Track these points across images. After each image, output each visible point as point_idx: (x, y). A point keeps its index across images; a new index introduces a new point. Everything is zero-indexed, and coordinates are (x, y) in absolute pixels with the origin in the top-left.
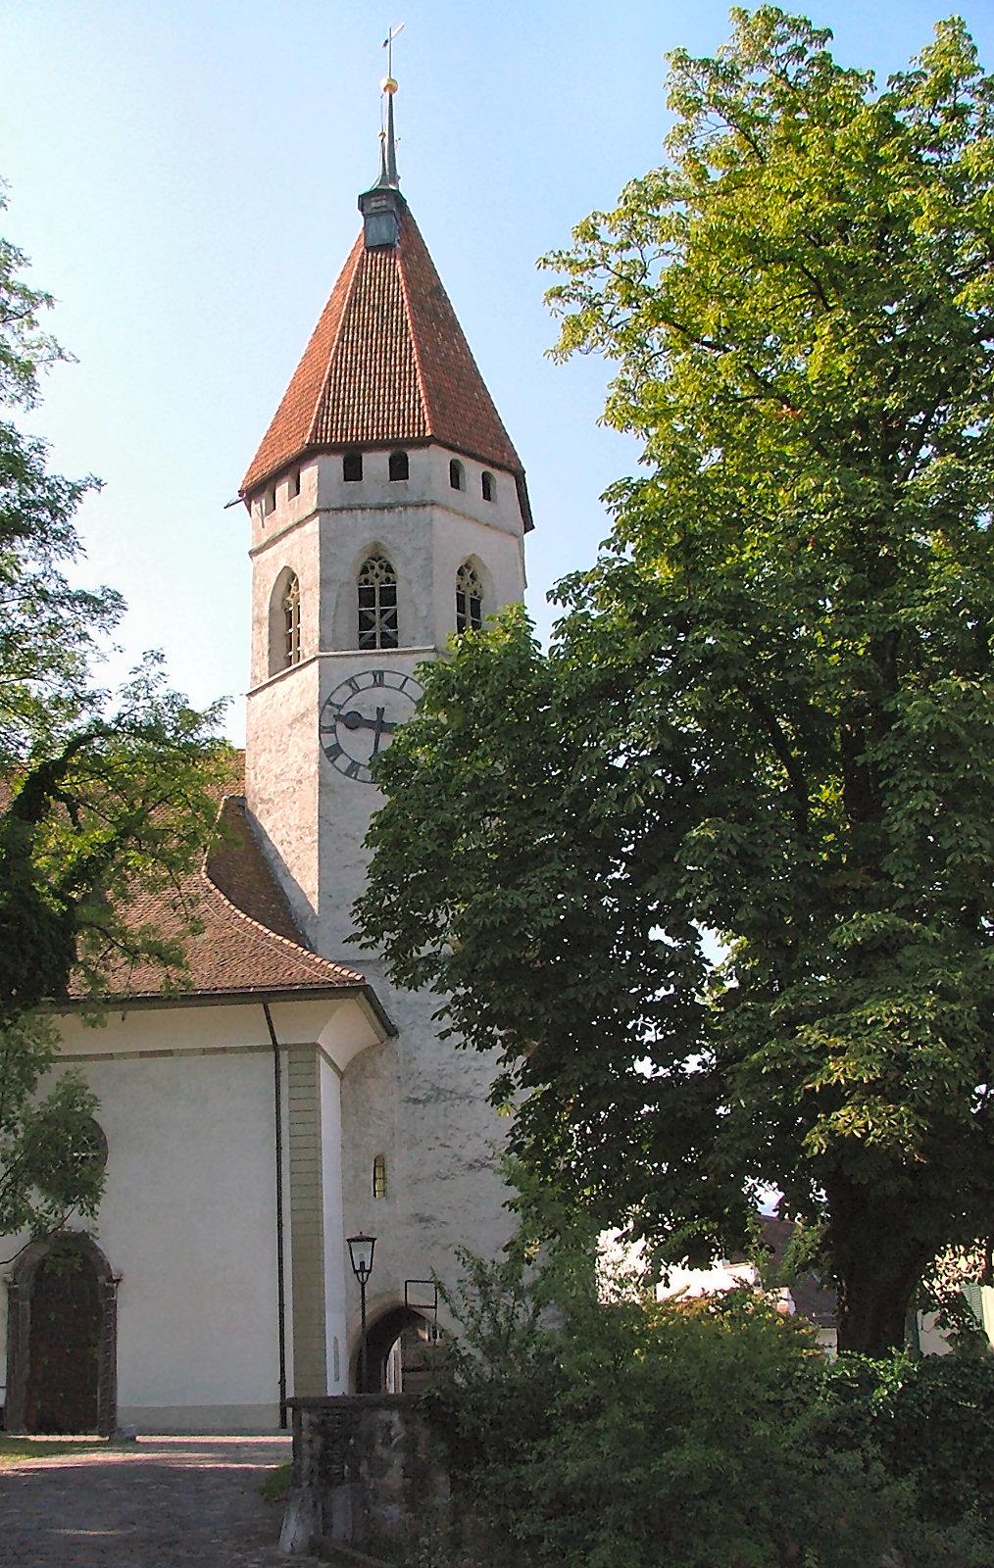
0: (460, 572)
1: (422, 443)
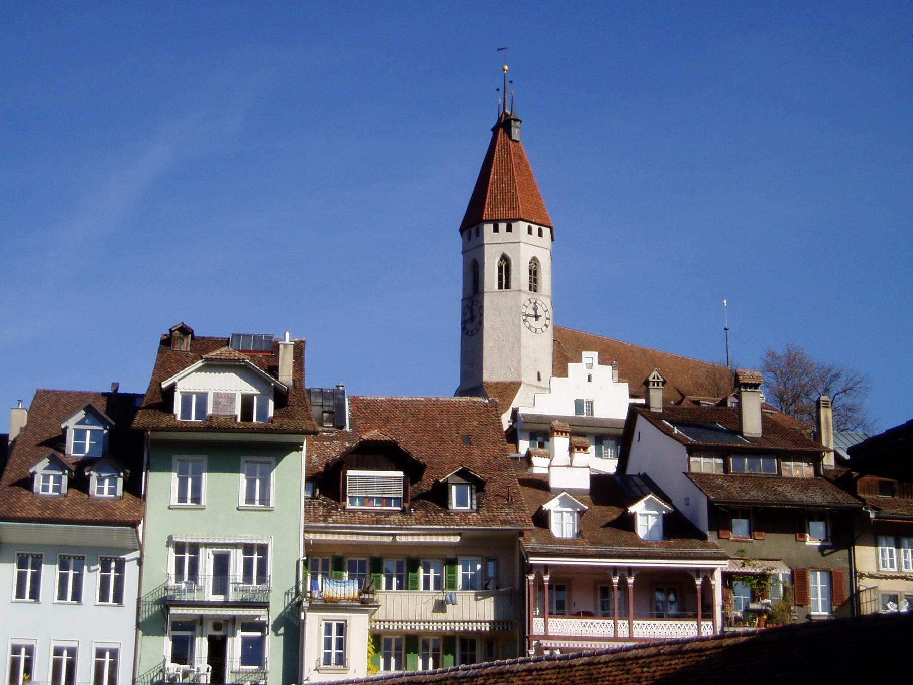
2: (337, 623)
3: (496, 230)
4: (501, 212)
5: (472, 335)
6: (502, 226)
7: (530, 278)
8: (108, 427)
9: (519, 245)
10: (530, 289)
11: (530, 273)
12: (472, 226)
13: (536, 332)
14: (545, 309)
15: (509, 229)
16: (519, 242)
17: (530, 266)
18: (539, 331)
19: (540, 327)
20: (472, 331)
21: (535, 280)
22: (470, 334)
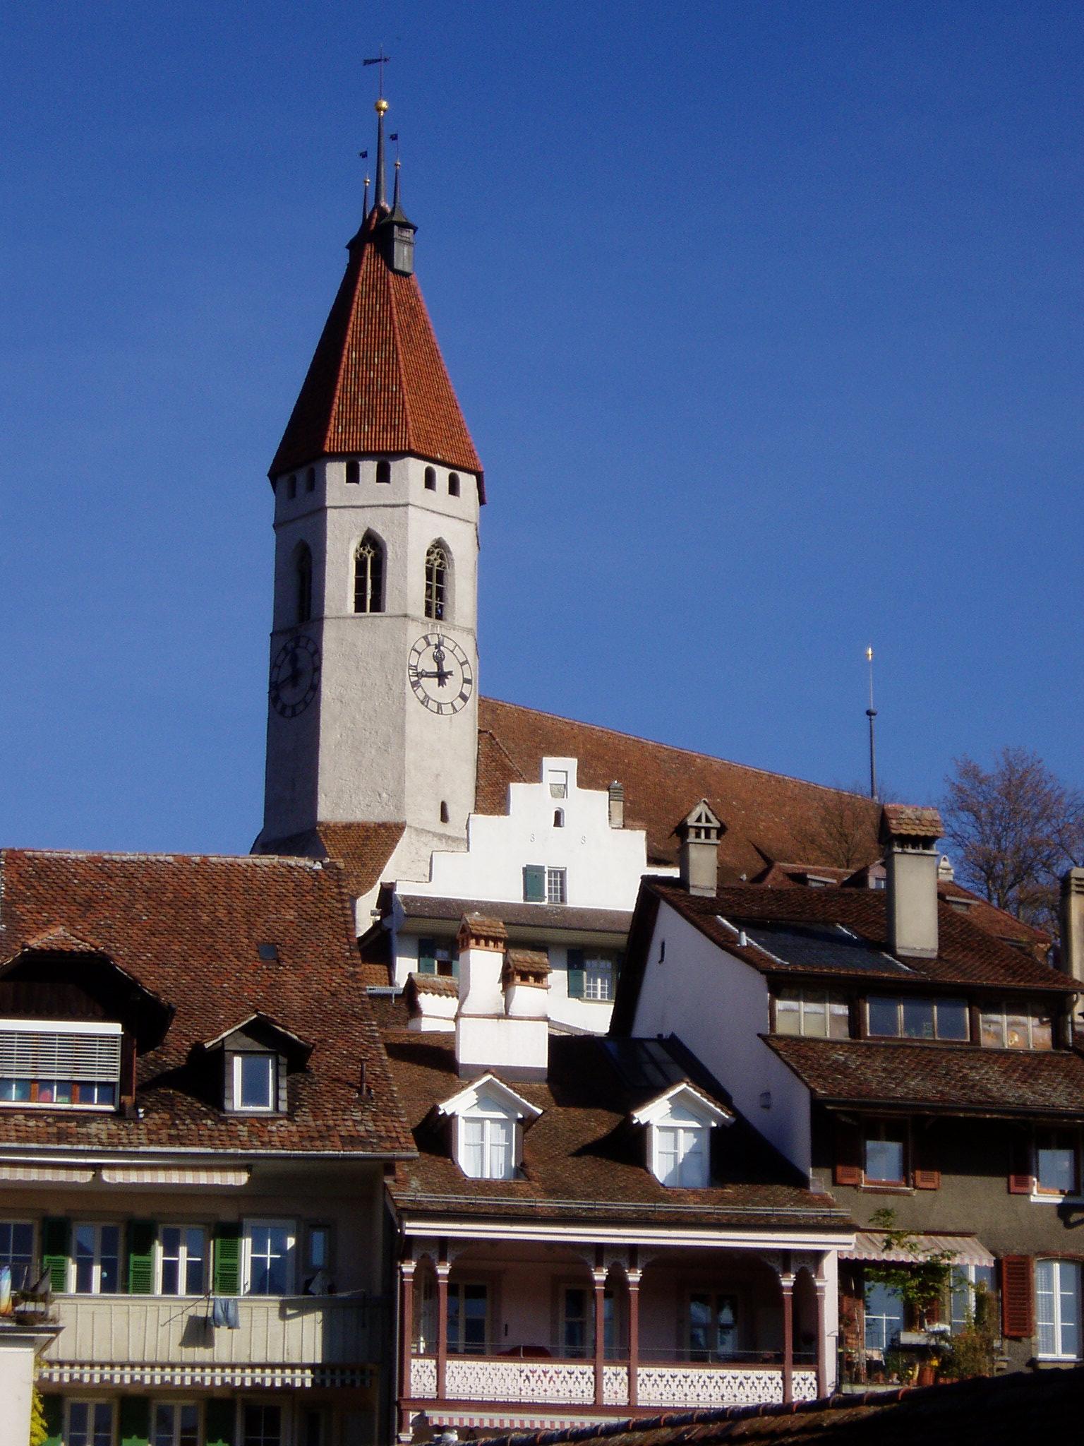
3: (353, 476)
4: (367, 437)
5: (294, 714)
6: (368, 468)
7: (429, 587)
10: (428, 614)
11: (429, 577)
13: (439, 710)
15: (383, 475)
16: (406, 505)
17: (428, 562)
18: (447, 709)
20: (294, 707)
21: (440, 594)
22: (288, 712)
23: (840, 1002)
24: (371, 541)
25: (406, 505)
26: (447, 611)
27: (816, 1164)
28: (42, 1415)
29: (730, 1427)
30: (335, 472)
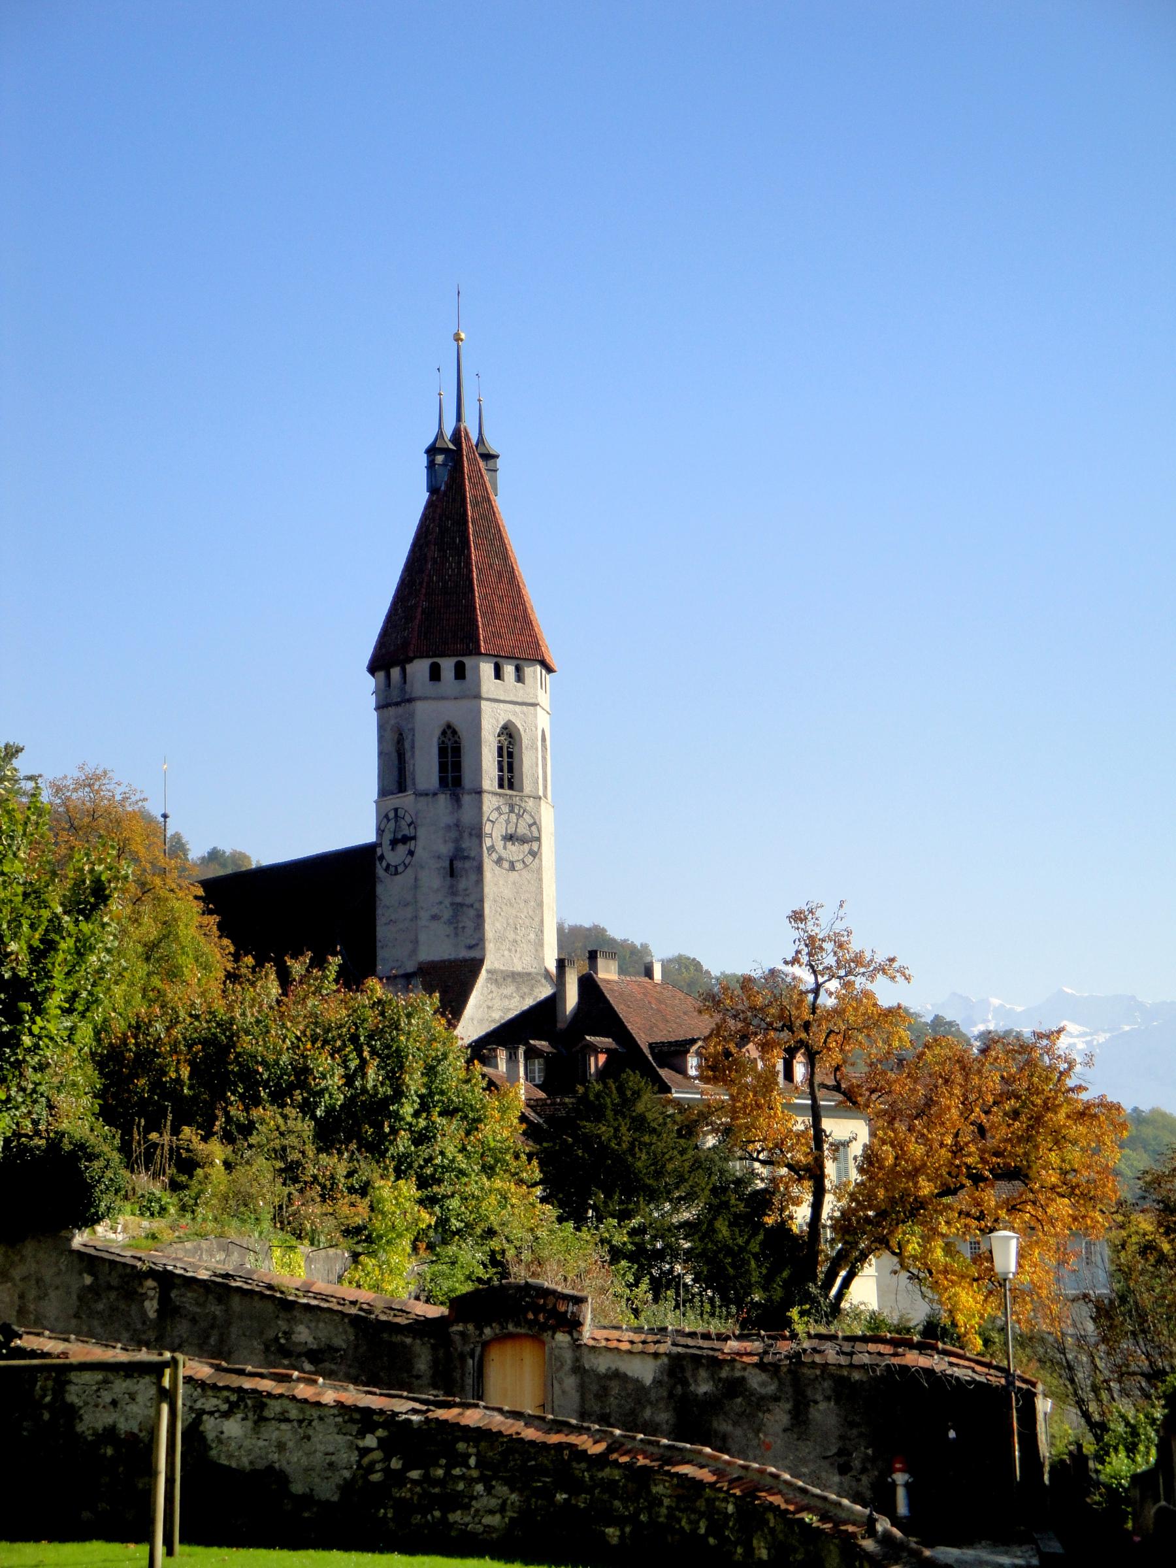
0: (444, 733)
1: (410, 660)
2: (181, 1542)
3: (498, 675)
4: (508, 643)
5: (396, 873)
6: (509, 670)
7: (500, 763)
8: (1137, 1539)
9: (536, 710)
10: (501, 786)
11: (500, 755)
12: (393, 665)
13: (512, 868)
14: (531, 821)
15: (520, 678)
16: (534, 705)
17: (499, 741)
18: (519, 866)
19: (520, 858)
20: (396, 867)
21: (511, 769)
22: (392, 869)
23: (545, 1040)
24: (509, 733)
25: (534, 705)
26: (516, 781)
27: (82, 1150)
28: (995, 1546)
29: (319, 1394)
30: (486, 669)
